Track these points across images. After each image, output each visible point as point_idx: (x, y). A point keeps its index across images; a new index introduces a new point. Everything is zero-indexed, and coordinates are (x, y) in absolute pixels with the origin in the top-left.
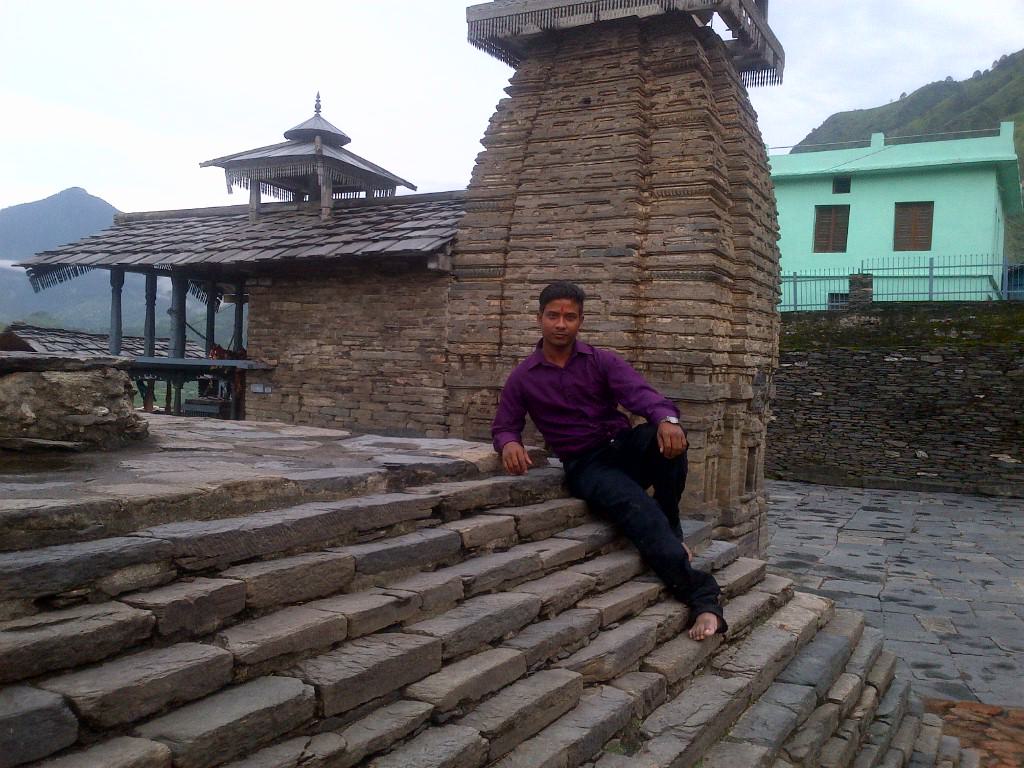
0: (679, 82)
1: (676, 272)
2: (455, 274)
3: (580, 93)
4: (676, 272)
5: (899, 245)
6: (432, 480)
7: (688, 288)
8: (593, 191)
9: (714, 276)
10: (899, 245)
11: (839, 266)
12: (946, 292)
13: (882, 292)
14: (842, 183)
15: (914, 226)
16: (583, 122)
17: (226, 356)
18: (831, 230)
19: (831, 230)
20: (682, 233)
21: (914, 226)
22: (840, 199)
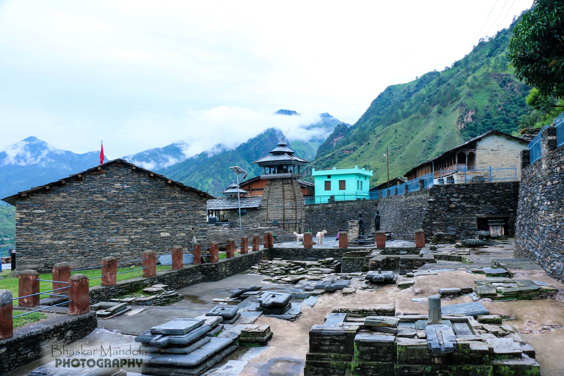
0: (287, 185)
1: (288, 209)
2: (261, 209)
3: (275, 186)
4: (288, 209)
5: (340, 189)
6: (122, 295)
7: (290, 211)
8: (278, 199)
9: (292, 209)
10: (340, 189)
11: (329, 193)
12: (347, 198)
13: (337, 199)
14: (329, 176)
15: (342, 185)
16: (276, 190)
17: (48, 188)
18: (328, 186)
19: (328, 186)
20: (288, 204)
21: (342, 185)
22: (329, 180)
